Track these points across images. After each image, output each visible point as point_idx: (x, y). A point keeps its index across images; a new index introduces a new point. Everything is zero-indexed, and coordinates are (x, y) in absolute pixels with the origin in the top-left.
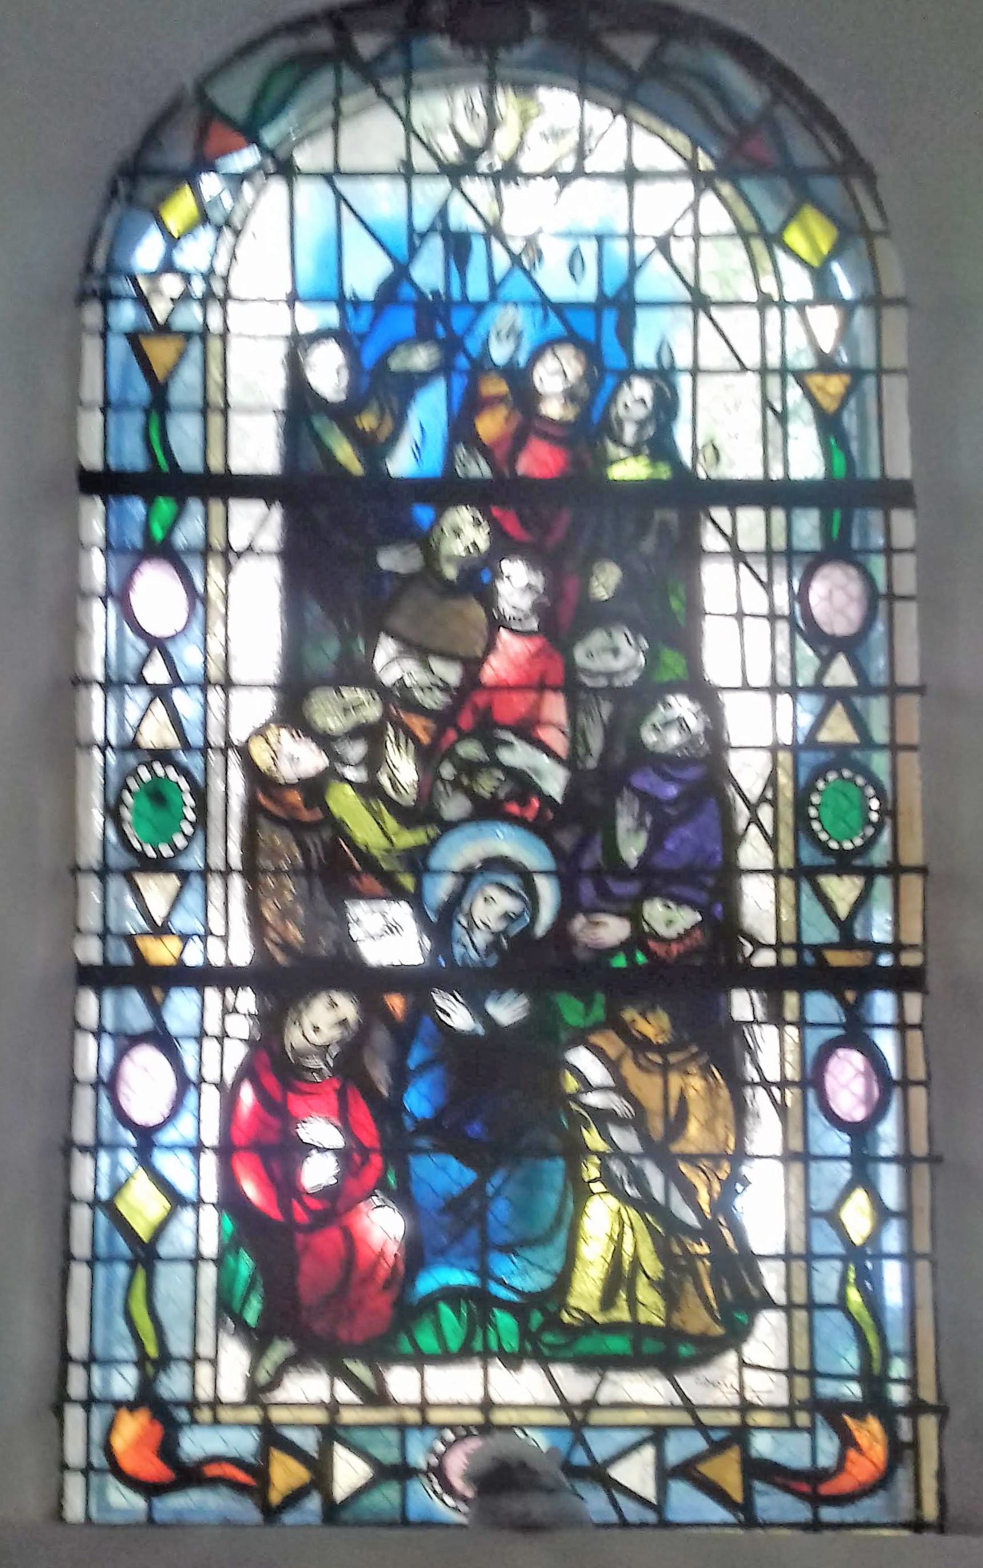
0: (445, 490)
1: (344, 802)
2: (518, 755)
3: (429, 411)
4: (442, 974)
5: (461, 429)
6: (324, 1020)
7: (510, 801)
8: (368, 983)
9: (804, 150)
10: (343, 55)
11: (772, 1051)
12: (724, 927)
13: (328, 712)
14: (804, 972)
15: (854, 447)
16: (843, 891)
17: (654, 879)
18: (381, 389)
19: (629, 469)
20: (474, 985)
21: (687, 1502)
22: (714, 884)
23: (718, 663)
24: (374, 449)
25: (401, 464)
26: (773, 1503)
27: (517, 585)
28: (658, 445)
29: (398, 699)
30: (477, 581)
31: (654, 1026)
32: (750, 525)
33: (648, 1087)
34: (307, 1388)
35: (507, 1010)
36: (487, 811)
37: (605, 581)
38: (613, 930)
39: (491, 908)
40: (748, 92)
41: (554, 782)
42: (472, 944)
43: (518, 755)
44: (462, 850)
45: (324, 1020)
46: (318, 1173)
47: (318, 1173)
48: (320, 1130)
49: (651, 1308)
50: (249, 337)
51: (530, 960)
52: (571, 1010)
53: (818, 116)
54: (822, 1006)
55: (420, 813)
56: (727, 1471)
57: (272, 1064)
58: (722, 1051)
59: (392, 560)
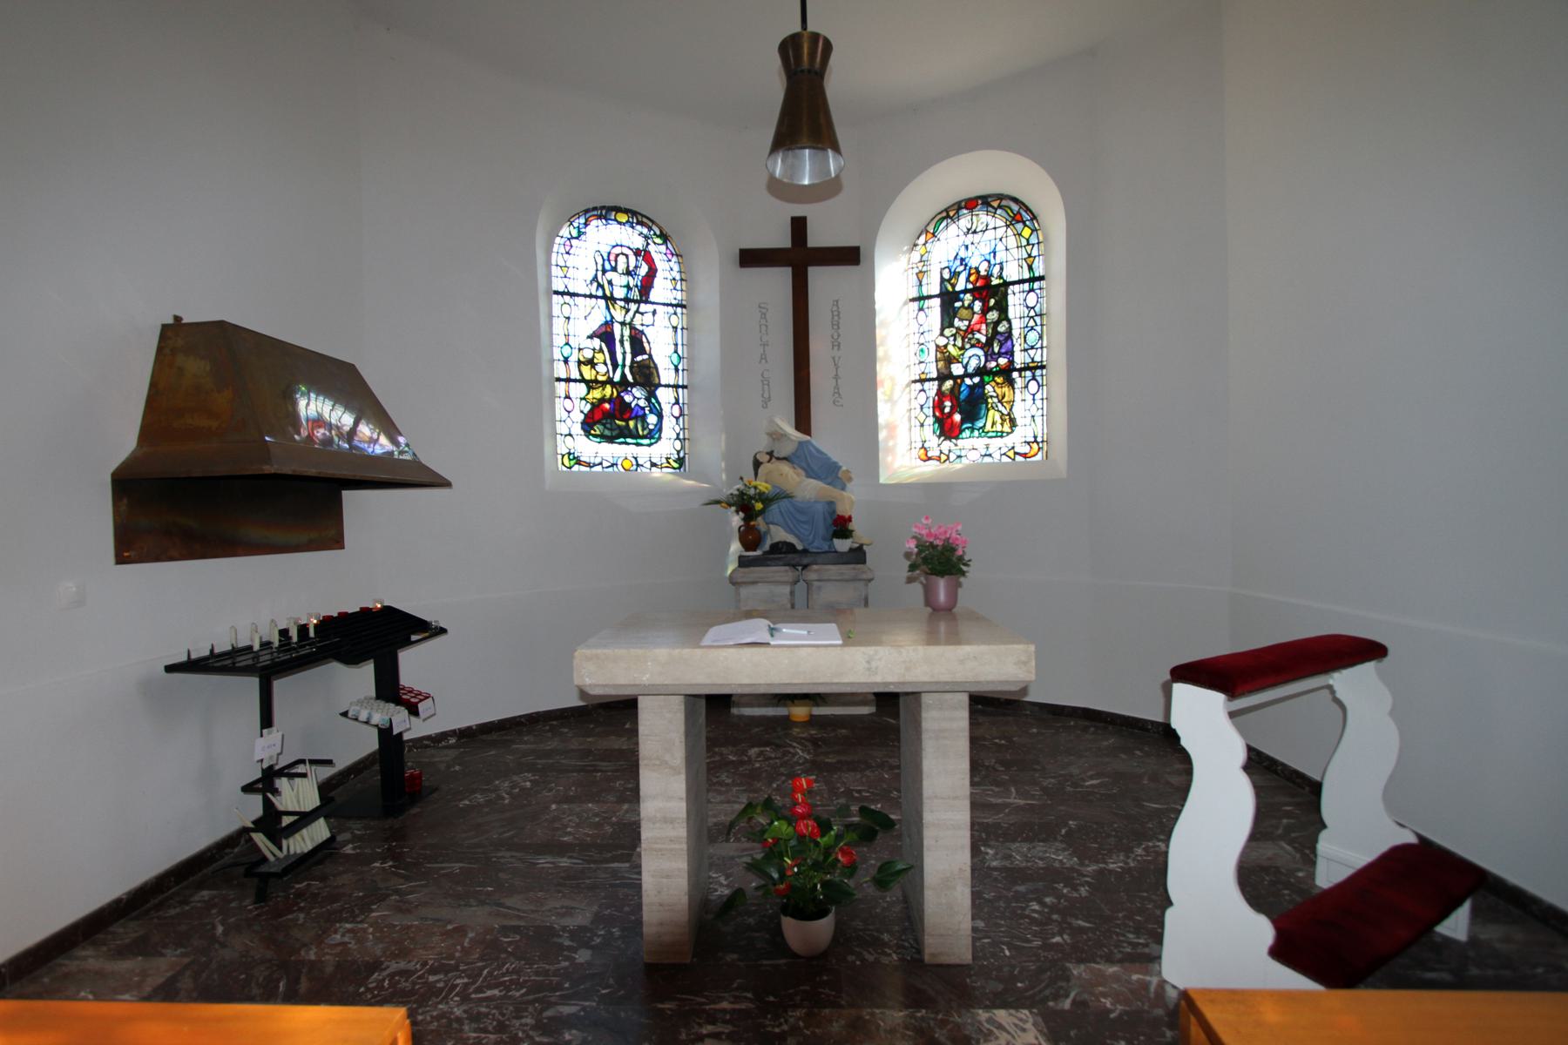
0: (965, 291)
1: (950, 348)
2: (977, 336)
3: (963, 277)
4: (966, 375)
5: (968, 280)
6: (949, 384)
7: (978, 344)
8: (955, 378)
9: (1026, 216)
10: (948, 216)
11: (1019, 383)
12: (1011, 362)
13: (947, 332)
14: (1027, 368)
15: (484, 737)
16: (1032, 352)
17: (1000, 354)
18: (955, 275)
19: (995, 282)
20: (971, 376)
21: (1005, 459)
22: (1010, 353)
23: (1011, 315)
24: (953, 286)
25: (958, 288)
26: (1019, 458)
27: (978, 306)
28: (1000, 277)
29: (958, 329)
30: (970, 307)
31: (999, 380)
32: (1016, 288)
33: (999, 391)
34: (947, 443)
35: (977, 380)
36: (973, 346)
37: (992, 302)
38: (993, 364)
39: (973, 364)
40: (1015, 207)
41: (983, 339)
42: (970, 370)
43: (977, 336)
44: (968, 354)
45: (949, 384)
46: (947, 410)
47: (947, 410)
48: (948, 404)
49: (998, 427)
50: (837, 387)
51: (981, 371)
52: (986, 379)
53: (1028, 210)
54: (1028, 373)
55: (962, 348)
56: (1011, 454)
57: (940, 393)
58: (1011, 383)
59: (958, 304)
